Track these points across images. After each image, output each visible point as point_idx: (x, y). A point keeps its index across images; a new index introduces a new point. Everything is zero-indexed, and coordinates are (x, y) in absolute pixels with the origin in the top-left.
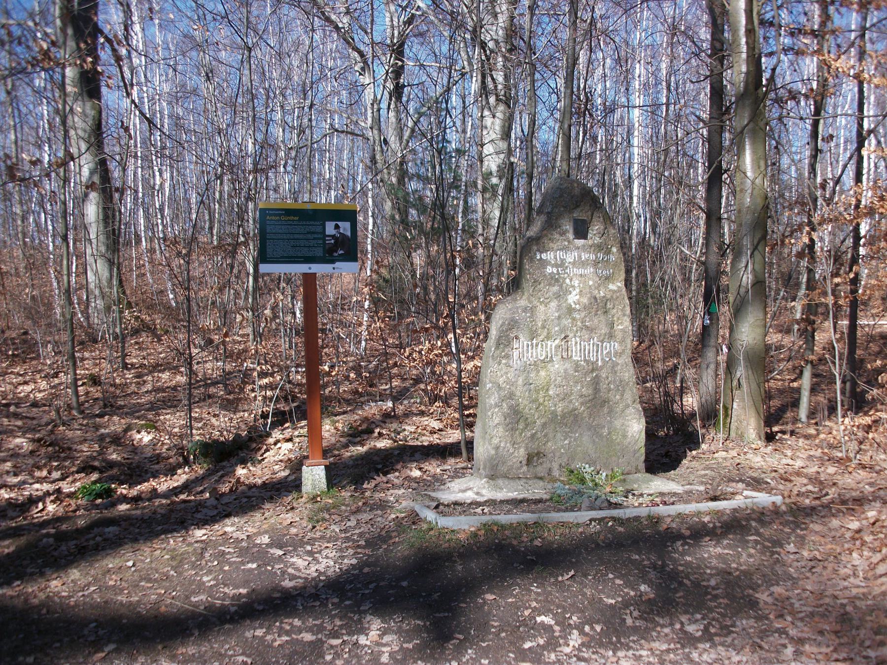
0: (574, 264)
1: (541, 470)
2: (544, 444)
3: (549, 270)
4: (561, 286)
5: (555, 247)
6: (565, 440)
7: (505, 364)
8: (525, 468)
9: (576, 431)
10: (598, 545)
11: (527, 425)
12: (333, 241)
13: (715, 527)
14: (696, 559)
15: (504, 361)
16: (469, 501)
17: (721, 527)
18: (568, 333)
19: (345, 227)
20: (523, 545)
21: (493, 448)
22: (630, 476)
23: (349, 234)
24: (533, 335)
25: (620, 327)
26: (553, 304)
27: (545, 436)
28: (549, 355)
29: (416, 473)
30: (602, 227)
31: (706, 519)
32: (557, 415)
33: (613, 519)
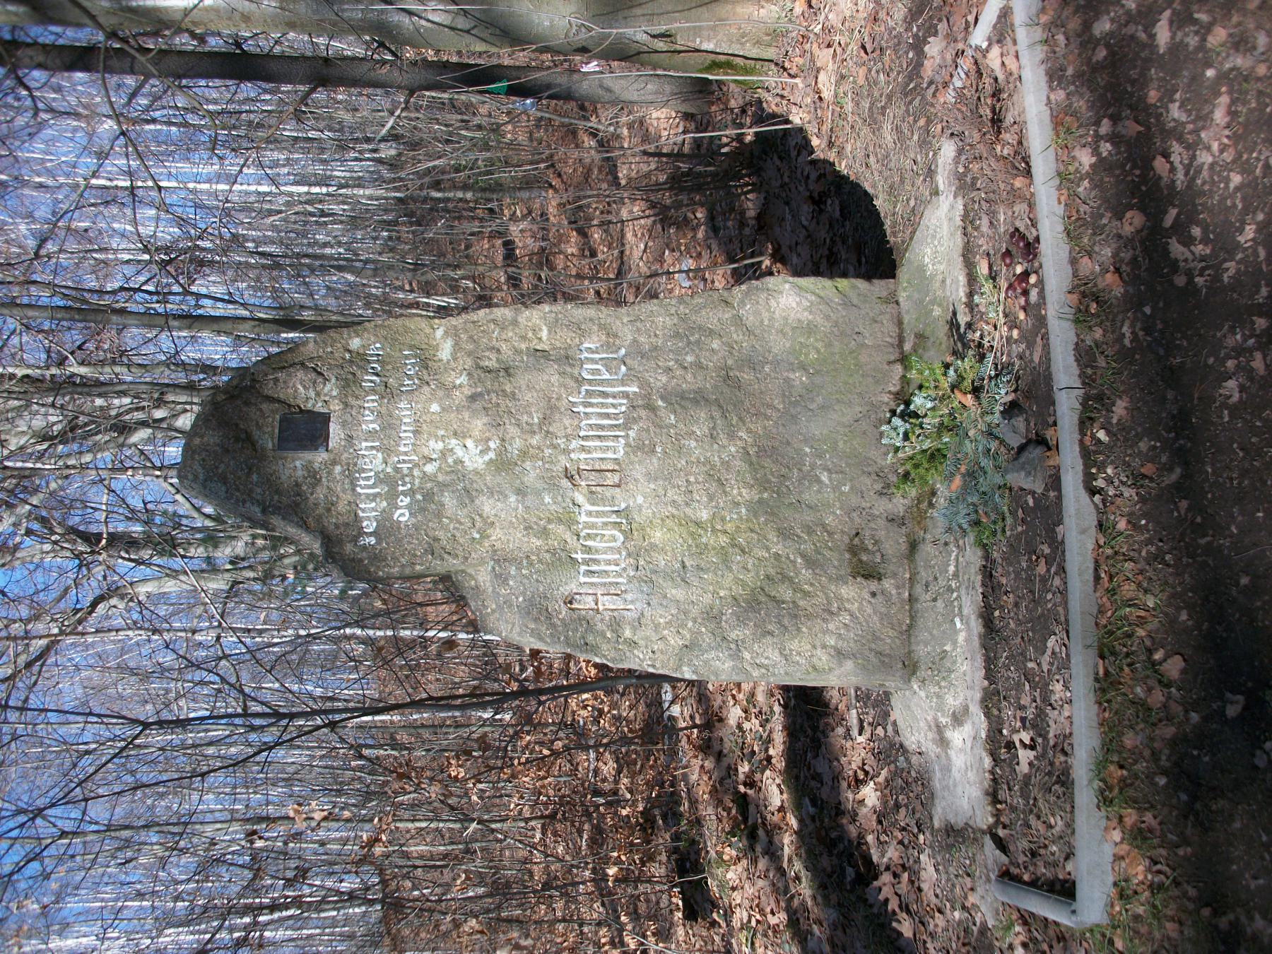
0: (387, 451)
1: (894, 543)
2: (830, 534)
3: (402, 515)
4: (443, 486)
5: (348, 497)
6: (819, 481)
7: (634, 629)
8: (888, 584)
9: (799, 451)
10: (1179, 489)
11: (785, 578)
13: (1114, 138)
14: (1247, 209)
15: (628, 633)
16: (988, 762)
17: (1115, 119)
18: (559, 468)
20: (1177, 709)
21: (840, 664)
22: (906, 319)
24: (563, 560)
25: (544, 334)
26: (488, 506)
27: (810, 531)
28: (614, 518)
29: (870, 795)
30: (300, 374)
31: (1085, 159)
32: (761, 501)
33: (1085, 422)
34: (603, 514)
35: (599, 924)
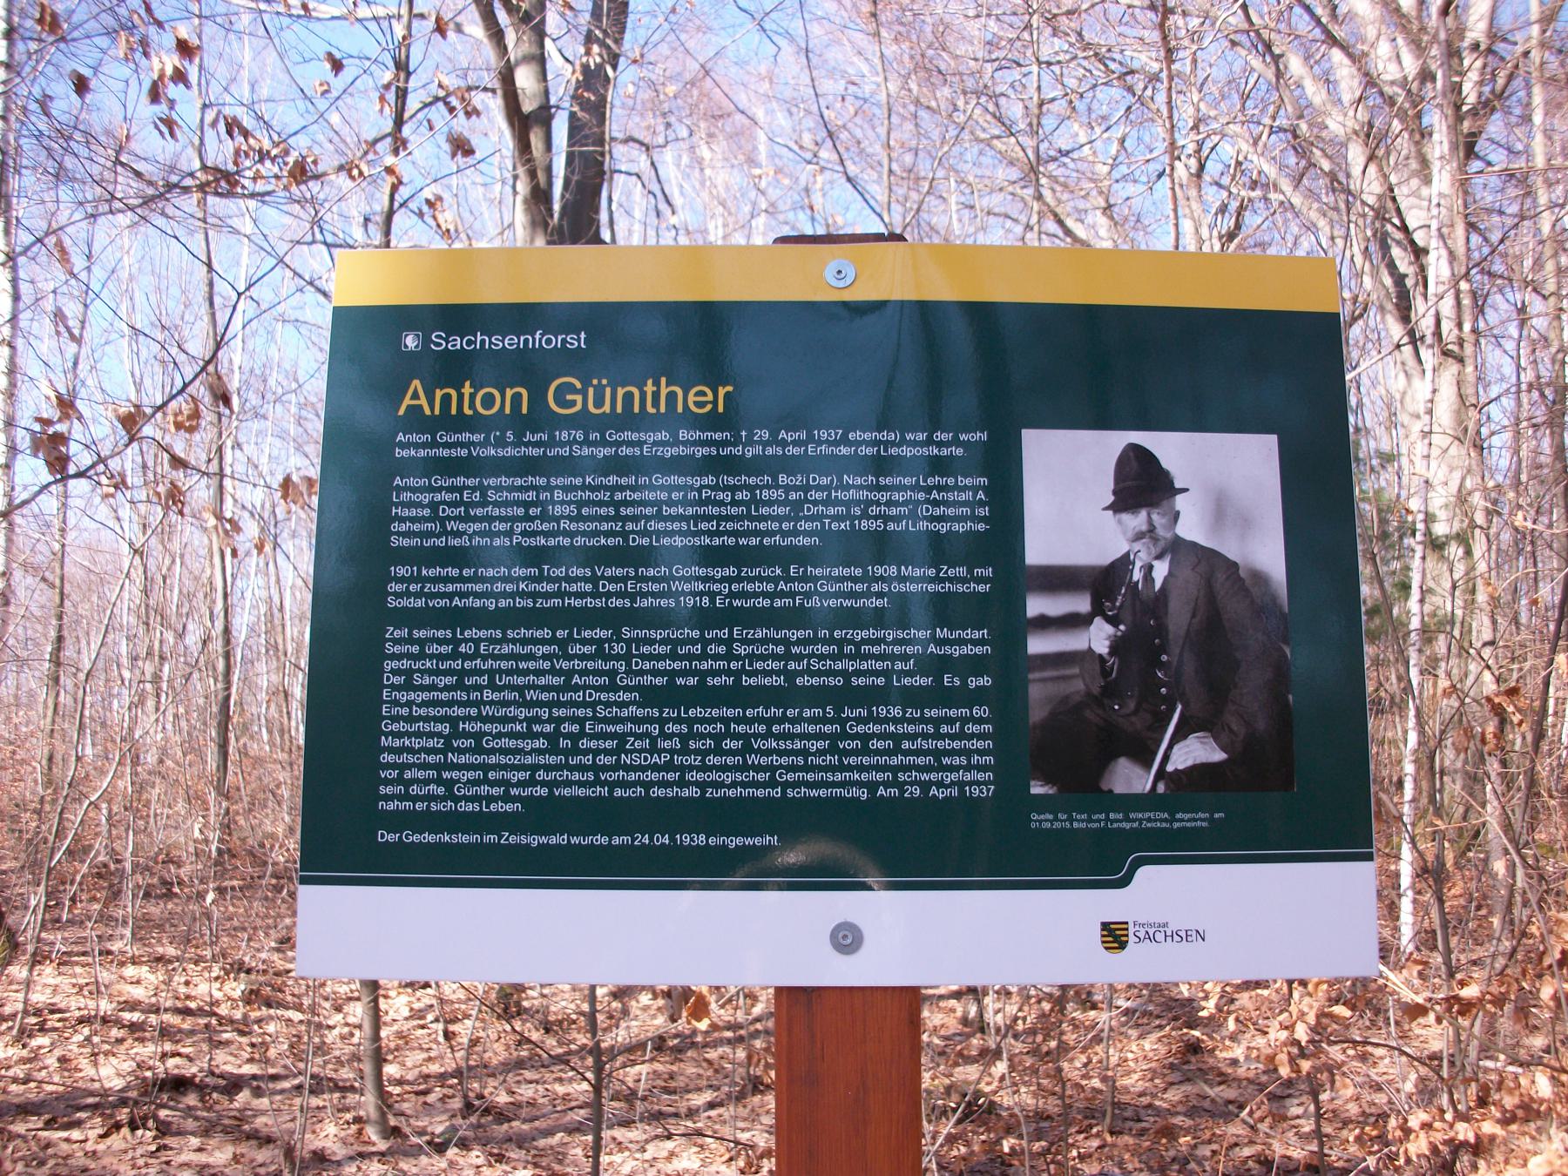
12: (1099, 637)
19: (1228, 483)
23: (1266, 553)
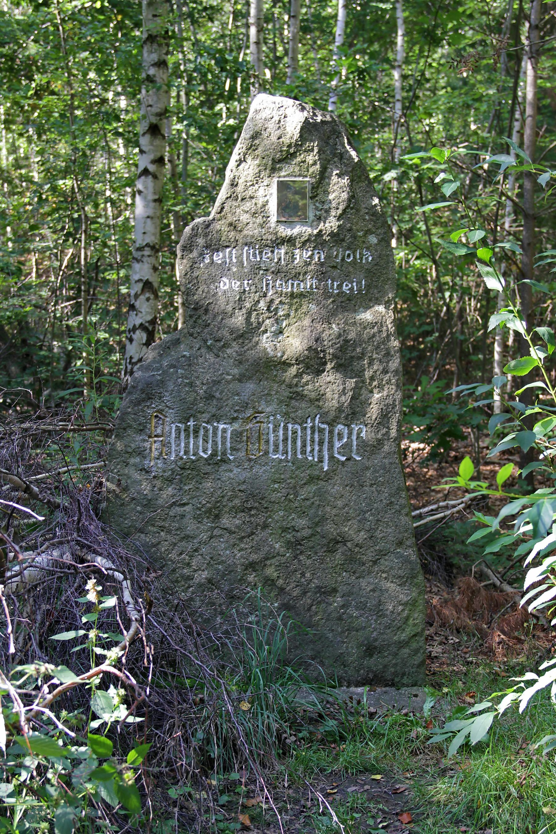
34: (224, 443)
35: (296, 557)
